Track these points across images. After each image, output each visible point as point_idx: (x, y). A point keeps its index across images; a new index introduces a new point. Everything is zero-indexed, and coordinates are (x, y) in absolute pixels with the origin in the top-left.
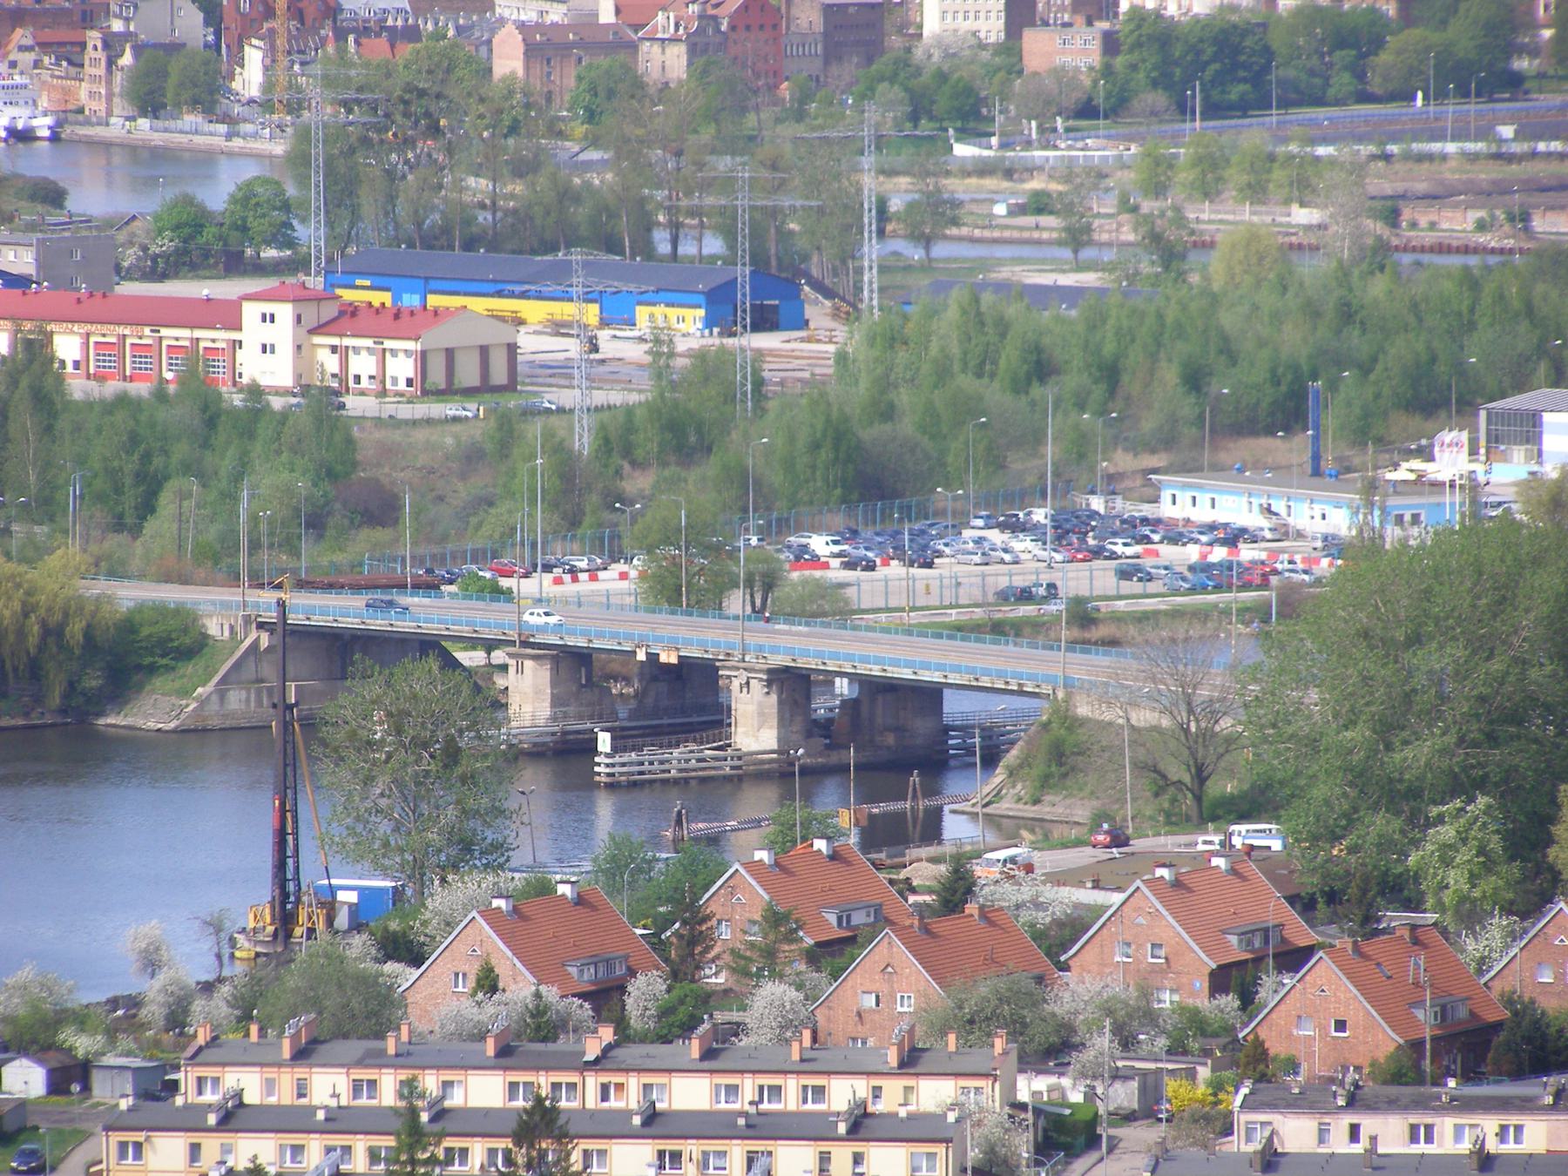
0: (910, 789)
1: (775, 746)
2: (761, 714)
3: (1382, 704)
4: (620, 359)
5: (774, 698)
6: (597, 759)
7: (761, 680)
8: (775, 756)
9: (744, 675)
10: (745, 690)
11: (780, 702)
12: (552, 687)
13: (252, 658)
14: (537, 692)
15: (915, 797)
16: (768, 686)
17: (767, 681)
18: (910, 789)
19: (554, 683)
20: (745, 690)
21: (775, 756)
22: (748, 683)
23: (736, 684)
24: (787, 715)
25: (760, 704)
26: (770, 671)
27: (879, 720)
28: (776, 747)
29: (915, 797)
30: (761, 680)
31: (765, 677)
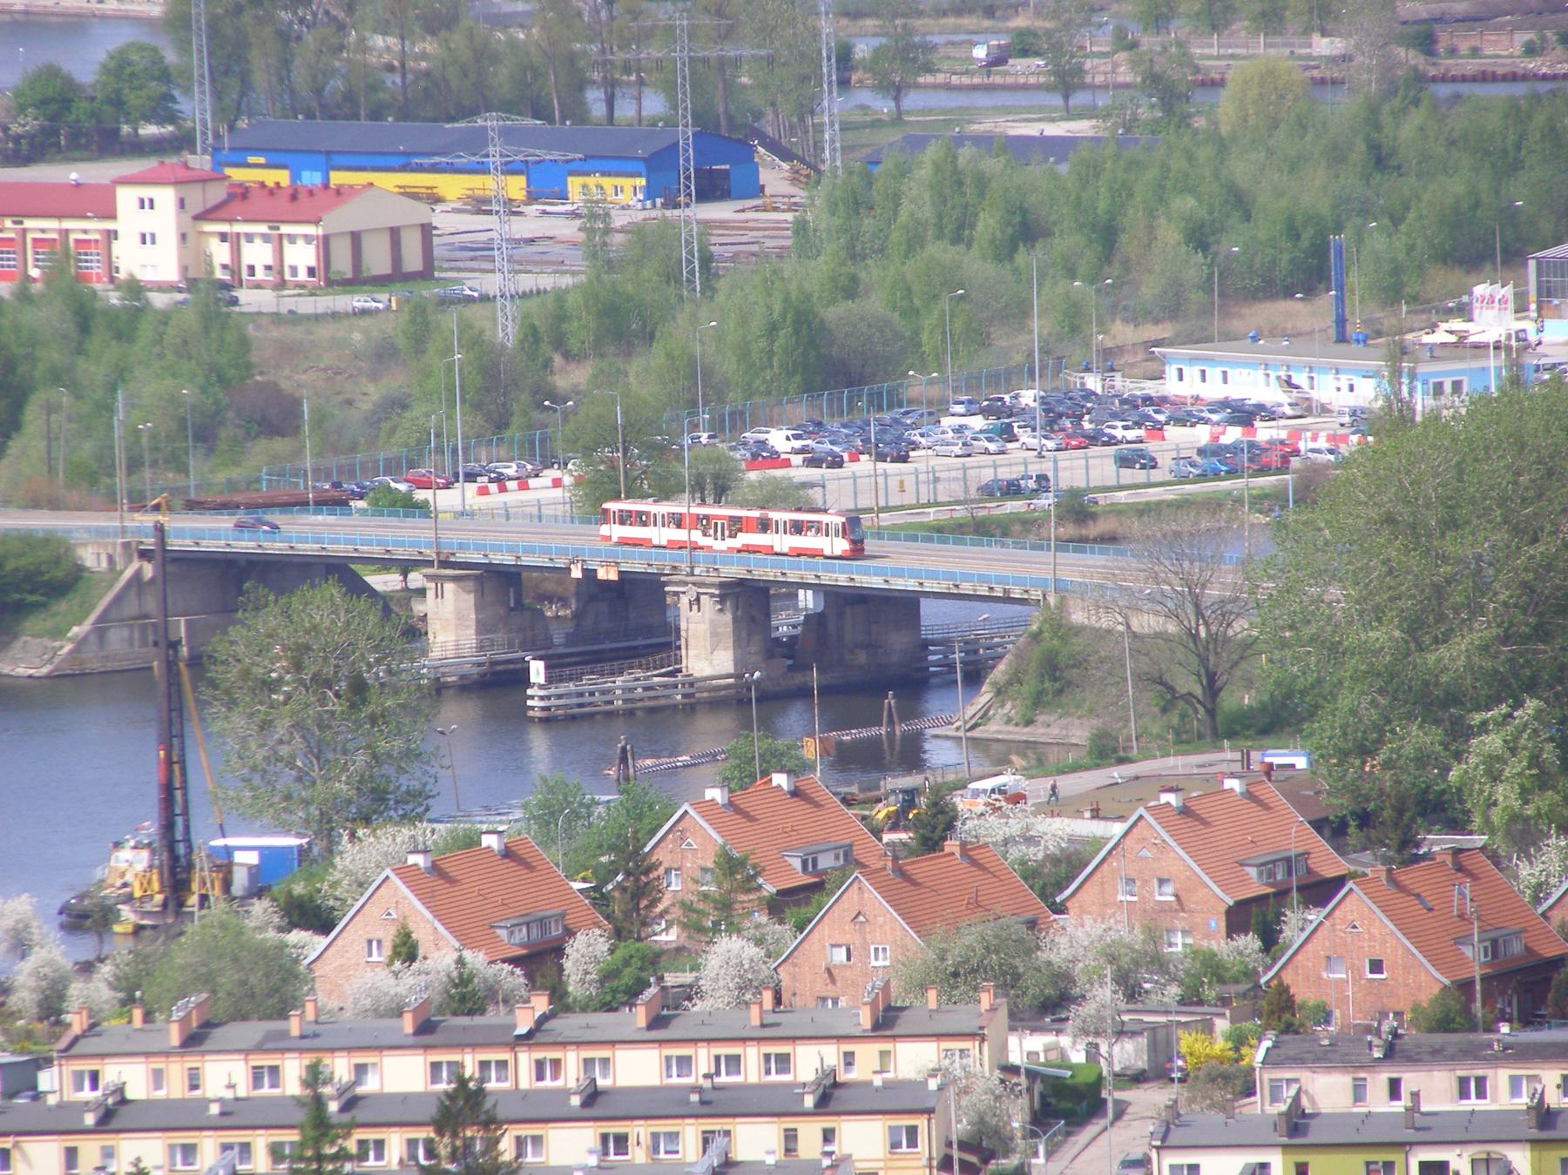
0: (885, 714)
2: (715, 634)
6: (529, 692)
7: (712, 596)
10: (695, 607)
11: (735, 620)
14: (460, 618)
15: (891, 722)
18: (885, 714)
20: (695, 607)
22: (698, 600)
23: (684, 600)
24: (744, 635)
29: (891, 722)
30: (712, 596)
31: (717, 592)
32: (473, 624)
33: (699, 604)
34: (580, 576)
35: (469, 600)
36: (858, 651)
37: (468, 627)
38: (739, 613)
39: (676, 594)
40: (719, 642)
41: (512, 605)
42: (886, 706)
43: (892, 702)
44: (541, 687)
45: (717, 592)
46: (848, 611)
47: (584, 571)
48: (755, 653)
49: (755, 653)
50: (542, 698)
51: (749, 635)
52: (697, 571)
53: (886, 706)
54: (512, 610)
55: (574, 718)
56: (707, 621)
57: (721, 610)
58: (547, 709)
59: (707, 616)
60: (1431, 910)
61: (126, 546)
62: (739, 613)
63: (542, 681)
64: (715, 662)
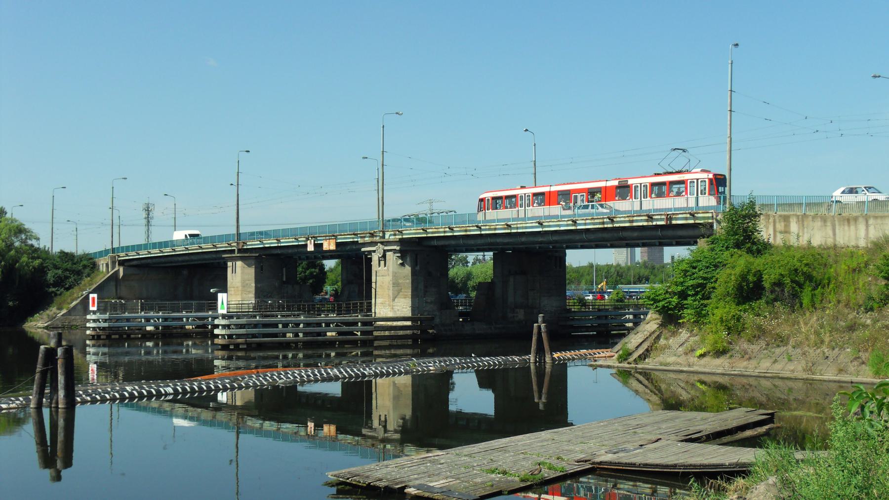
0: (534, 338)
1: (408, 313)
2: (396, 284)
3: (519, 464)
4: (648, 323)
5: (408, 269)
6: (88, 317)
7: (395, 251)
8: (409, 323)
9: (380, 248)
10: (382, 263)
11: (414, 273)
12: (256, 282)
13: (113, 283)
14: (244, 285)
15: (540, 351)
16: (402, 257)
17: (400, 251)
18: (534, 338)
19: (257, 280)
20: (382, 263)
21: (409, 323)
22: (384, 256)
23: (375, 258)
24: (421, 286)
25: (395, 276)
26: (402, 242)
27: (511, 299)
28: (409, 314)
29: (540, 351)
30: (395, 251)
31: (398, 248)
32: (253, 289)
33: (385, 260)
34: (313, 249)
35: (251, 272)
36: (518, 310)
37: (249, 292)
38: (418, 268)
39: (370, 252)
40: (399, 291)
41: (284, 279)
42: (544, 397)
43: (543, 326)
44: (94, 313)
45: (398, 248)
46: (512, 279)
47: (315, 245)
48: (431, 303)
49: (431, 303)
50: (224, 327)
51: (426, 287)
52: (387, 237)
53: (535, 331)
54: (284, 283)
55: (260, 347)
56: (391, 274)
57: (402, 265)
58: (230, 336)
59: (391, 270)
60: (149, 197)
61: (113, 258)
62: (418, 268)
63: (95, 309)
64: (396, 308)
